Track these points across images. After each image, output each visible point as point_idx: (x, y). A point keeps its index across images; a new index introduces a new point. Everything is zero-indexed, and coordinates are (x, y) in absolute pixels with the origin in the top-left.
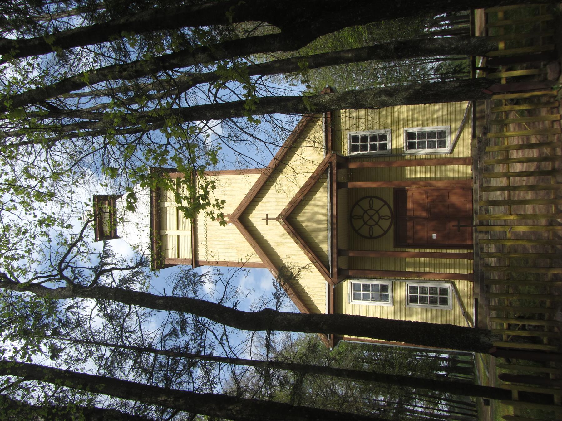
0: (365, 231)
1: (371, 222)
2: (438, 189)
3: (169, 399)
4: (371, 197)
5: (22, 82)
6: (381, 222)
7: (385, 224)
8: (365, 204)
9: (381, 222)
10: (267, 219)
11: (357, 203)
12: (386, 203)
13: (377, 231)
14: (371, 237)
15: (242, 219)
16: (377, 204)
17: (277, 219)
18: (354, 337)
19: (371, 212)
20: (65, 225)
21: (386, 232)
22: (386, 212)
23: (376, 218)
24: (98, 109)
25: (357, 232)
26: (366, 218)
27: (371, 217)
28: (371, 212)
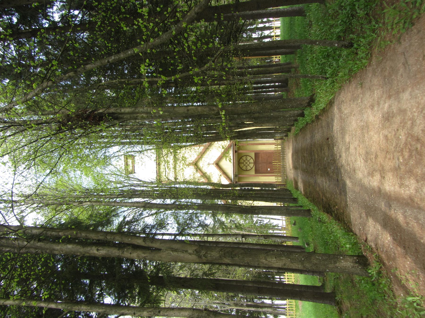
0: (244, 168)
1: (246, 165)
2: (333, 147)
3: (173, 78)
4: (246, 156)
5: (64, 33)
6: (250, 165)
7: (252, 165)
8: (244, 158)
9: (250, 165)
10: (209, 164)
11: (241, 158)
12: (252, 158)
13: (249, 168)
14: (247, 170)
15: (195, 164)
16: (249, 158)
17: (213, 164)
18: (202, 187)
19: (246, 161)
20: (398, 119)
21: (252, 168)
22: (252, 161)
23: (248, 163)
24: (188, 227)
25: (241, 168)
26: (245, 163)
27: (246, 163)
28: (246, 161)
